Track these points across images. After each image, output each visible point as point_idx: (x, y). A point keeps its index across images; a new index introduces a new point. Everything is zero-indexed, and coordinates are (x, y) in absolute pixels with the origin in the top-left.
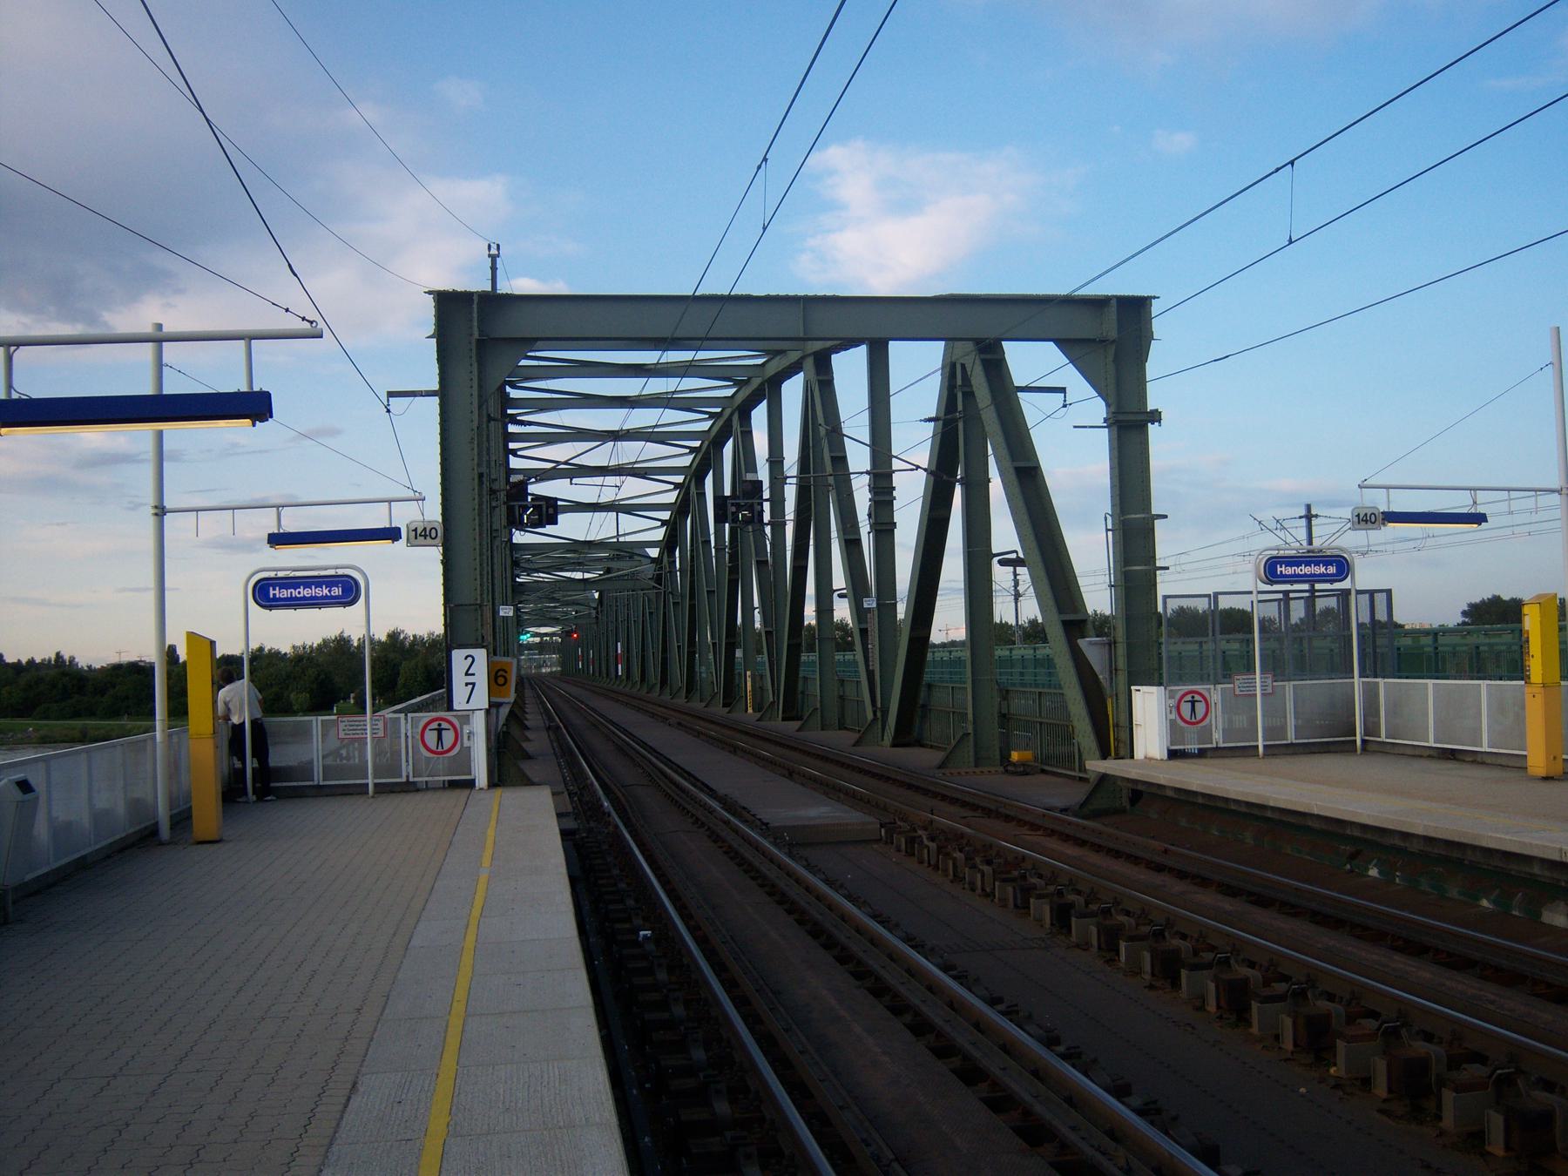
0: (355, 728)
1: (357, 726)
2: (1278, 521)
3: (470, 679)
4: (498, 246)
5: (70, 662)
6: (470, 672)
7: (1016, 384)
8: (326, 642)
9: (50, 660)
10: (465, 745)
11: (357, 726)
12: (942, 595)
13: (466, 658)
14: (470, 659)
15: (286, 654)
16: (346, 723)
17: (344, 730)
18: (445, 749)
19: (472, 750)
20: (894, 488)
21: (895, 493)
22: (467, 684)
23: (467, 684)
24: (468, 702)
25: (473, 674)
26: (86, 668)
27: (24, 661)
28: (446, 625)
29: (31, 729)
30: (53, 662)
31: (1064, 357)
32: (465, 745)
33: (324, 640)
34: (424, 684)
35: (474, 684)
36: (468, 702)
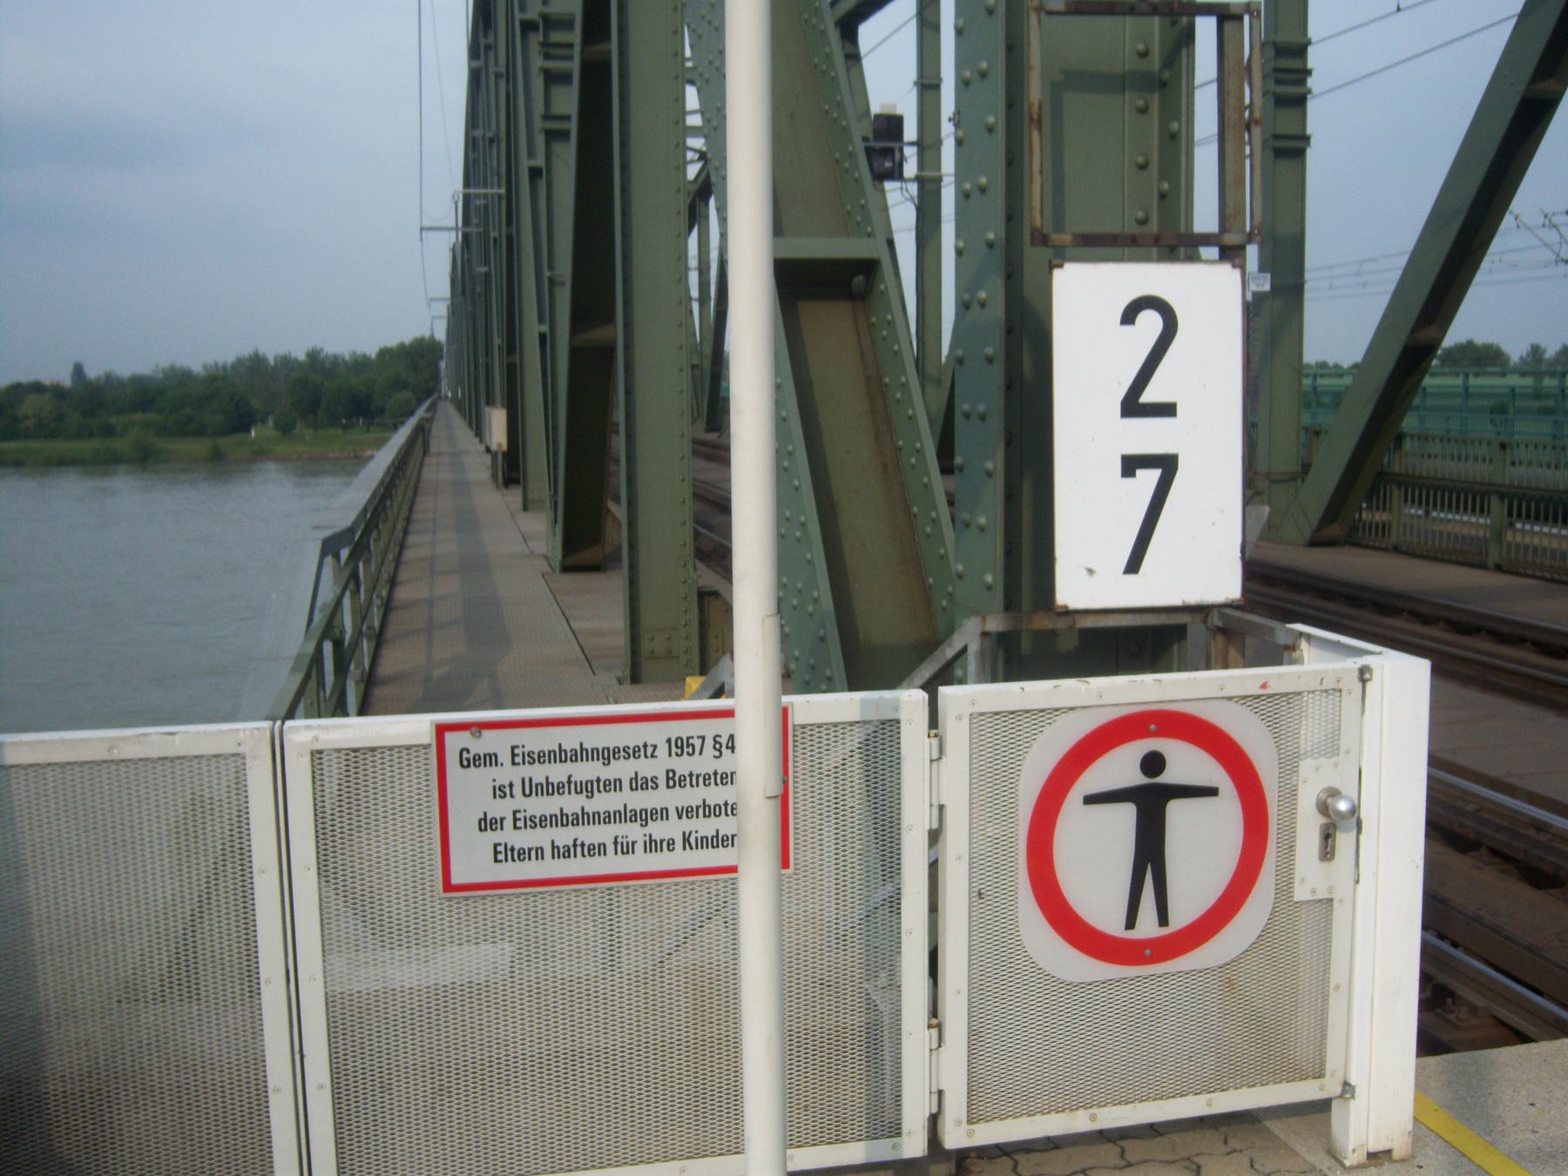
0: (572, 803)
1: (588, 788)
2: (1546, 216)
3: (1149, 436)
6: (1149, 396)
8: (240, 362)
10: (1301, 893)
11: (588, 788)
13: (1129, 316)
14: (1150, 322)
16: (506, 773)
17: (487, 824)
18: (1184, 912)
19: (1339, 914)
20: (1308, 72)
21: (1311, 82)
22: (1131, 465)
23: (1131, 465)
24: (1133, 565)
25: (1167, 410)
28: (465, 282)
32: (1301, 893)
35: (1167, 465)
36: (1133, 565)
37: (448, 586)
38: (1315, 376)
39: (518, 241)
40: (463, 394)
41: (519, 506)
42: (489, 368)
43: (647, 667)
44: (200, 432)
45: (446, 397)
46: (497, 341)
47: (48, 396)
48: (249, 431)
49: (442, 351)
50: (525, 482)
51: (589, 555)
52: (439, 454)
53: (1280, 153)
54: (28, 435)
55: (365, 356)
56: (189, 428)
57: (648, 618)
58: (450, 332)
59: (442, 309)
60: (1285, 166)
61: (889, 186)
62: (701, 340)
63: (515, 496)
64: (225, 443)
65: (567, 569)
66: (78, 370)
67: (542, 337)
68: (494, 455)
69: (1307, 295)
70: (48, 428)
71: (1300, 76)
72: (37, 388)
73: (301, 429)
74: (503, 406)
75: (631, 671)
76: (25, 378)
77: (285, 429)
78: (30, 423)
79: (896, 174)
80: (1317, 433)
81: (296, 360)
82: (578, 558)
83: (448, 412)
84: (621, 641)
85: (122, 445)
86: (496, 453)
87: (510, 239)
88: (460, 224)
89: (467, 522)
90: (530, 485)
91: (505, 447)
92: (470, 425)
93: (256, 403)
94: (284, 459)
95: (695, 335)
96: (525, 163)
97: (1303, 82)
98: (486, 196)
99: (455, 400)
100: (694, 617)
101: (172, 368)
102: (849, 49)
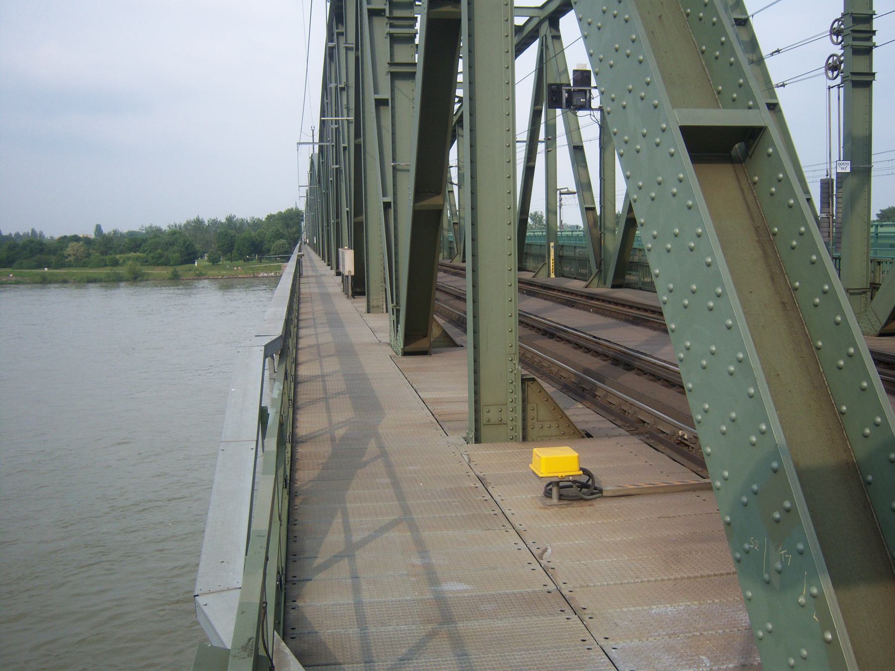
4: (314, 127)
5: (40, 234)
7: (456, 95)
9: (28, 233)
12: (519, 147)
15: (165, 230)
20: (874, 32)
21: (875, 39)
26: (49, 238)
27: (13, 234)
29: (11, 275)
30: (30, 235)
31: (575, 188)
33: (187, 221)
34: (250, 248)
37: (332, 366)
38: (877, 226)
39: (364, 148)
40: (318, 240)
41: (365, 309)
42: (338, 226)
43: (485, 431)
44: (166, 264)
45: (305, 243)
46: (345, 209)
47: (81, 243)
48: (194, 263)
49: (303, 216)
50: (368, 295)
51: (422, 344)
52: (308, 277)
53: (856, 84)
54: (70, 266)
55: (259, 220)
56: (160, 261)
57: (485, 398)
58: (309, 204)
59: (304, 191)
60: (860, 92)
61: (580, 113)
62: (459, 208)
63: (361, 302)
64: (181, 269)
65: (406, 353)
66: (98, 228)
67: (347, 211)
68: (344, 278)
69: (873, 173)
70: (82, 262)
71: (868, 35)
72: (76, 238)
73: (223, 261)
74: (350, 248)
75: (475, 434)
76: (69, 234)
77: (214, 261)
78: (72, 258)
79: (587, 106)
80: (879, 263)
81: (221, 223)
82: (412, 347)
83: (309, 251)
84: (465, 409)
85: (122, 270)
86: (347, 277)
87: (358, 147)
88: (317, 139)
89: (334, 321)
90: (371, 297)
91: (353, 273)
92: (323, 259)
93: (198, 247)
94: (214, 279)
95: (455, 206)
96: (370, 98)
97: (870, 39)
98: (337, 122)
99: (311, 244)
100: (519, 395)
101: (151, 227)
102: (554, 33)
